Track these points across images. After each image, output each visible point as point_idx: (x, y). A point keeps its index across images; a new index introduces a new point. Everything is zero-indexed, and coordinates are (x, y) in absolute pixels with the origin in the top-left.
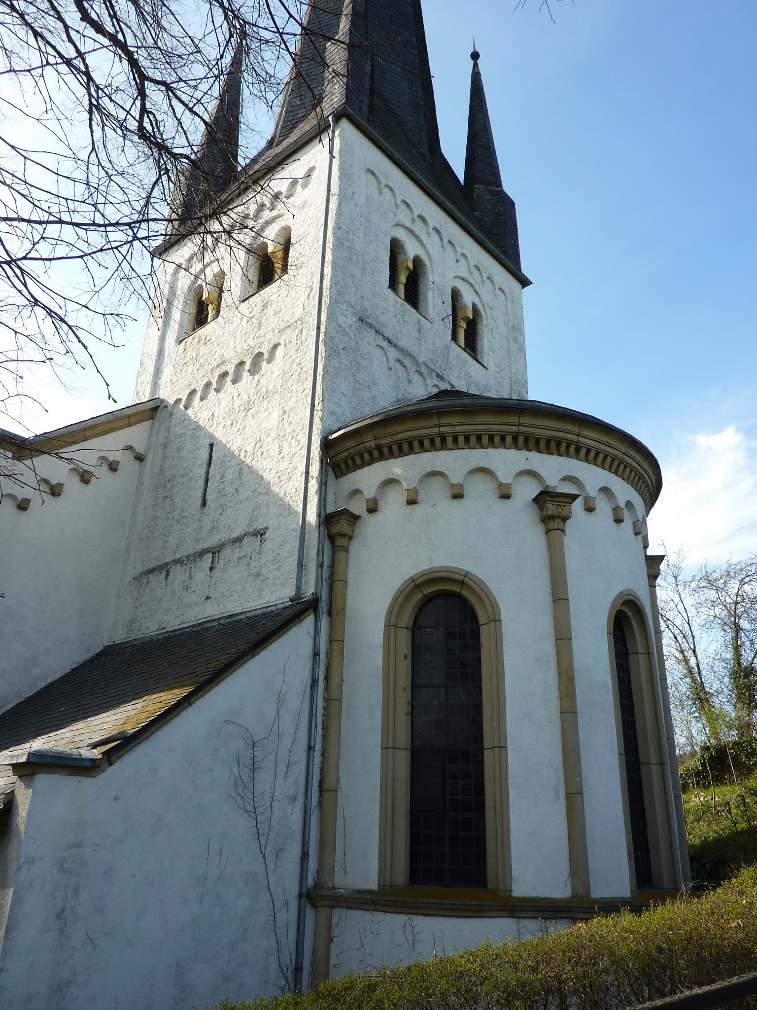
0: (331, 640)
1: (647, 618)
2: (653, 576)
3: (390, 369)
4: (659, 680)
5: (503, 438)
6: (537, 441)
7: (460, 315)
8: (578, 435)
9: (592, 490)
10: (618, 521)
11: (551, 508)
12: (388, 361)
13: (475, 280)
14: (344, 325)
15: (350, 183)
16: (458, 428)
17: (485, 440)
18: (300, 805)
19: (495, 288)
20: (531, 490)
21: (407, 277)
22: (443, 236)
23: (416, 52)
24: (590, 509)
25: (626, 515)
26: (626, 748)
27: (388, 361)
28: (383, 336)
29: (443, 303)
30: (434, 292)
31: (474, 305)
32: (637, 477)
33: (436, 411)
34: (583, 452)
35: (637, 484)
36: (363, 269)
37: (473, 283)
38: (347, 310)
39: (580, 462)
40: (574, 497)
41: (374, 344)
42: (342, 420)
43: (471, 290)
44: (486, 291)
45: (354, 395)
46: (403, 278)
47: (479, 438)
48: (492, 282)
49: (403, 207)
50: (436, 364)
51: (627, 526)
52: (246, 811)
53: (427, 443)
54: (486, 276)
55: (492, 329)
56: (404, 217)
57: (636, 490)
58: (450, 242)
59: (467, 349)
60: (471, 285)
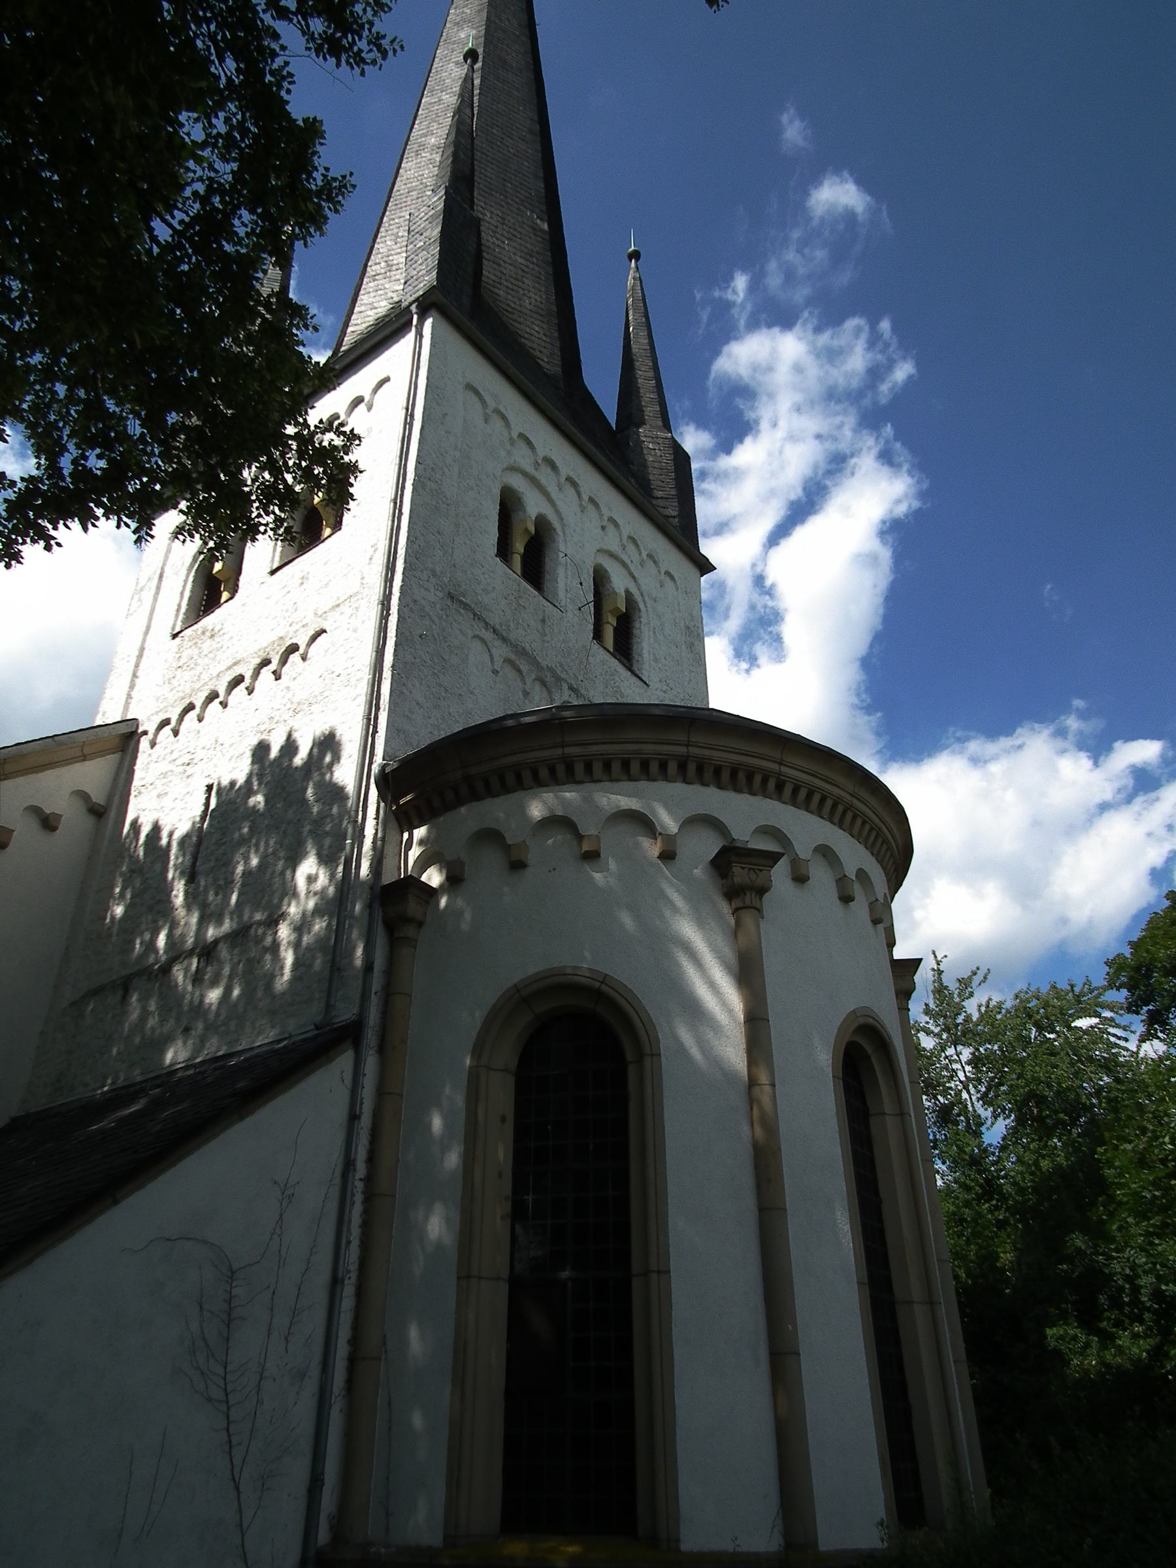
0: (381, 1092)
1: (898, 1061)
2: (905, 993)
3: (495, 672)
4: (920, 1161)
5: (663, 766)
6: (718, 771)
7: (607, 606)
8: (780, 764)
9: (803, 849)
10: (846, 899)
11: (740, 874)
12: (492, 660)
13: (630, 557)
14: (423, 602)
15: (440, 401)
16: (594, 749)
17: (635, 767)
18: (312, 1385)
19: (659, 571)
20: (711, 846)
21: (529, 541)
22: (582, 489)
23: (546, 227)
24: (800, 878)
25: (857, 890)
26: (871, 1274)
27: (492, 660)
28: (486, 624)
29: (581, 584)
30: (566, 569)
31: (627, 592)
32: (874, 834)
33: (557, 721)
34: (788, 789)
35: (873, 844)
36: (457, 526)
37: (628, 561)
38: (428, 581)
39: (783, 805)
40: (774, 858)
41: (470, 633)
42: (415, 744)
43: (624, 572)
44: (567, 502)
45: (437, 707)
46: (519, 546)
47: (626, 765)
48: (655, 562)
49: (521, 444)
50: (570, 672)
51: (860, 906)
52: (209, 1400)
53: (544, 773)
54: (646, 553)
55: (654, 628)
56: (612, 542)
57: (872, 854)
58: (591, 500)
59: (616, 653)
60: (624, 565)
